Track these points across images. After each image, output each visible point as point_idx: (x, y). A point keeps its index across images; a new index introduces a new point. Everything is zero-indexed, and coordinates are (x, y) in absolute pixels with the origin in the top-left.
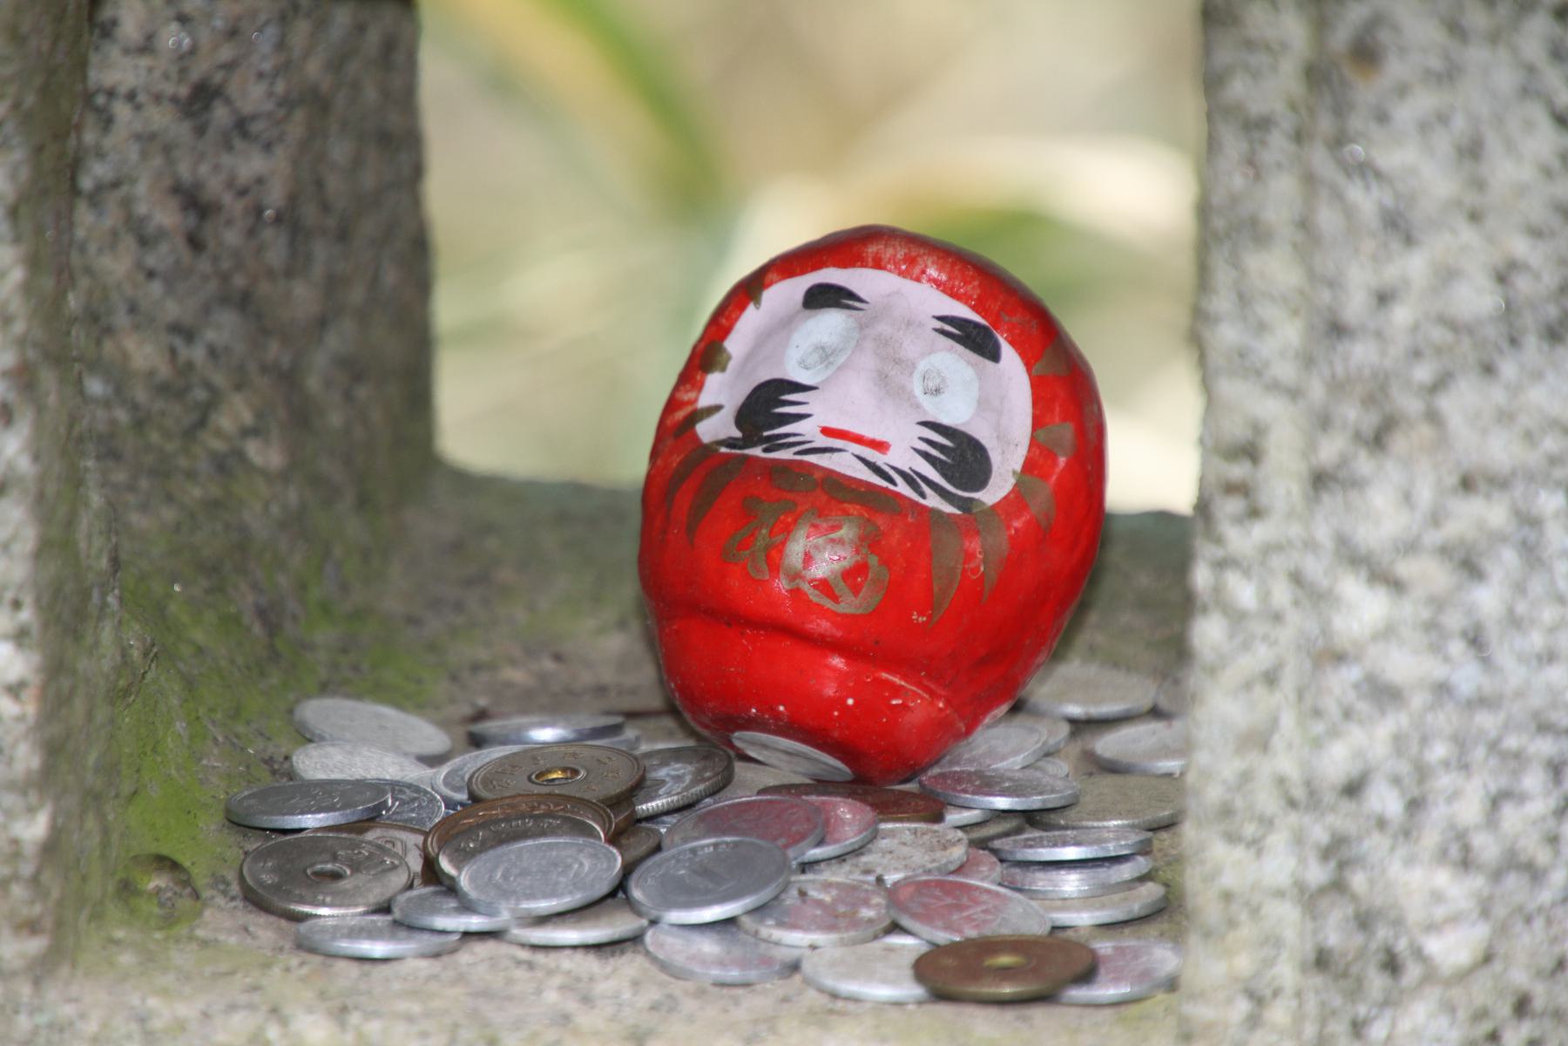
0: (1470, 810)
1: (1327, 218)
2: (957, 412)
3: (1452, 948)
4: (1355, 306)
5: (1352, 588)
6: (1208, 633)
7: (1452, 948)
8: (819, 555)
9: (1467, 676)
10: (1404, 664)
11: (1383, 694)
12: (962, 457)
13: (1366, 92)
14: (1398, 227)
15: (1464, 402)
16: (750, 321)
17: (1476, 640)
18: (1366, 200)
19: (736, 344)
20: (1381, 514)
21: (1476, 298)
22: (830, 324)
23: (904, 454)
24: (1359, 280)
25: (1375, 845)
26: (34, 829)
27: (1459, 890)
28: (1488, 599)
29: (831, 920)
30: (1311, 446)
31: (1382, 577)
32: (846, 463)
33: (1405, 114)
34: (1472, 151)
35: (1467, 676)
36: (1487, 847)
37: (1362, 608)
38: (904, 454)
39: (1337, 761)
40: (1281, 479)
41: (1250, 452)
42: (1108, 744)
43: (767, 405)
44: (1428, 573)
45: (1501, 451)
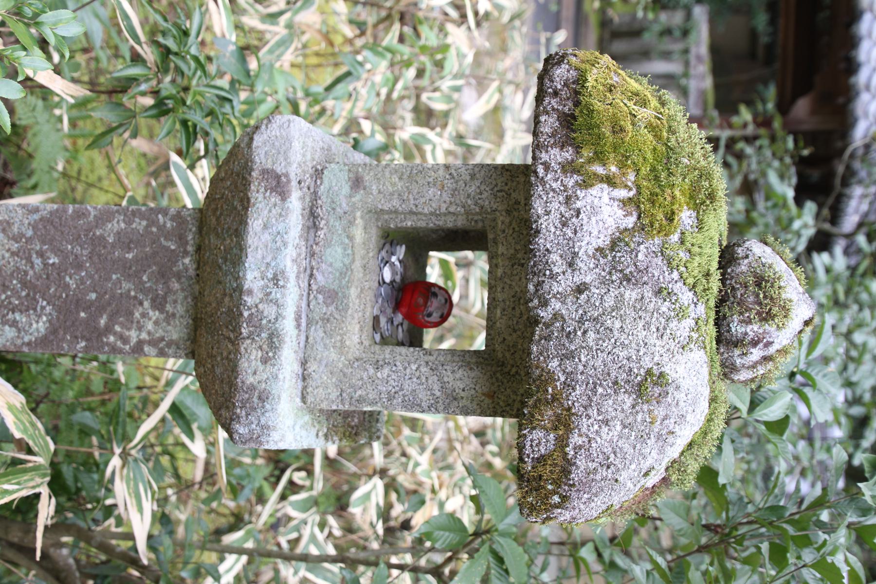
0: (393, 377)
1: (454, 364)
2: (434, 315)
3: (379, 374)
4: (445, 367)
5: (416, 366)
6: (412, 349)
7: (379, 374)
8: (421, 301)
9: (407, 377)
10: (408, 371)
11: (405, 369)
12: (430, 315)
13: (467, 369)
14: (453, 372)
15: (435, 378)
16: (444, 292)
17: (410, 378)
18: (456, 369)
19: (442, 291)
20: (424, 369)
21: (446, 379)
22: (443, 301)
23: (430, 309)
24: (448, 368)
25: (390, 367)
26: (392, 226)
27: (385, 376)
28: (415, 380)
29: (382, 305)
30: (444, 59)
31: (417, 369)
32: (429, 303)
33: (465, 373)
34: (461, 379)
35: (407, 377)
36: (389, 379)
37: (414, 367)
38: (430, 309)
39: (398, 364)
40: (427, 358)
41: (430, 355)
42: (400, 328)
43: (435, 295)
44: (417, 374)
45: (430, 382)
